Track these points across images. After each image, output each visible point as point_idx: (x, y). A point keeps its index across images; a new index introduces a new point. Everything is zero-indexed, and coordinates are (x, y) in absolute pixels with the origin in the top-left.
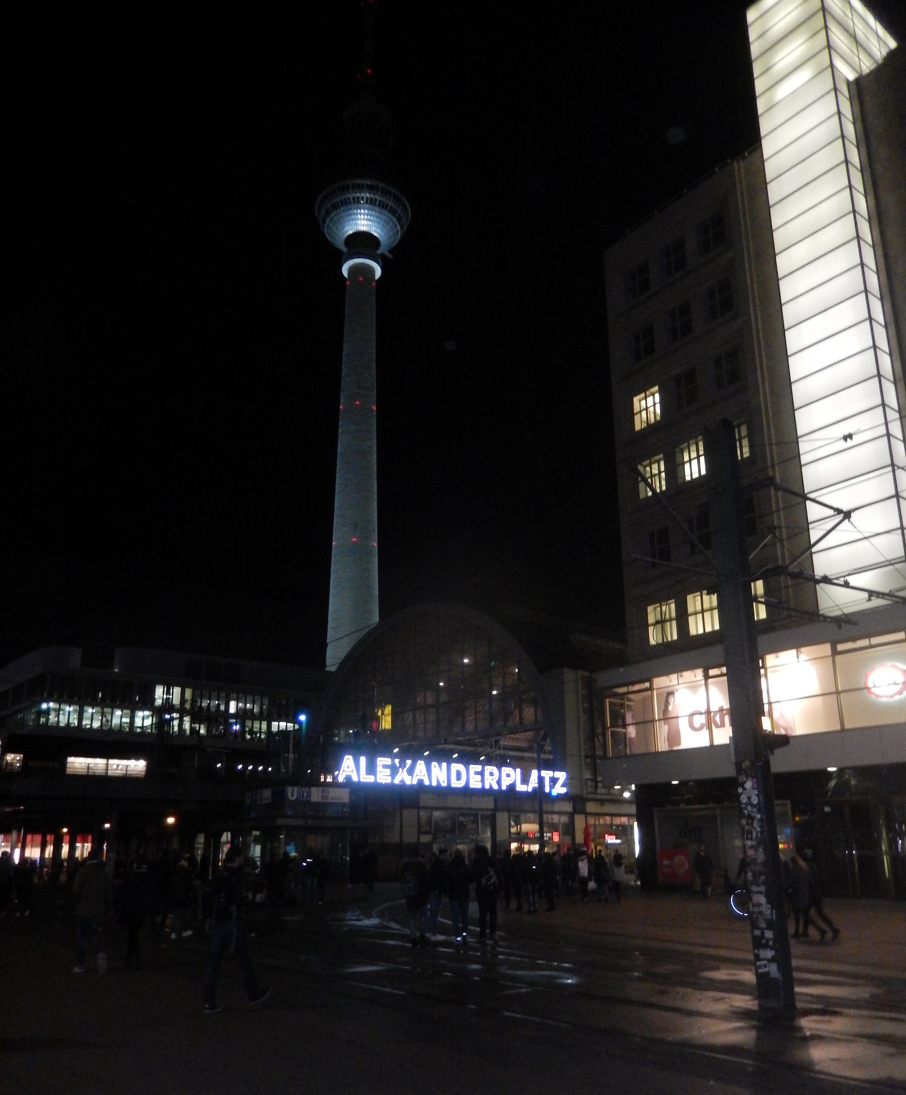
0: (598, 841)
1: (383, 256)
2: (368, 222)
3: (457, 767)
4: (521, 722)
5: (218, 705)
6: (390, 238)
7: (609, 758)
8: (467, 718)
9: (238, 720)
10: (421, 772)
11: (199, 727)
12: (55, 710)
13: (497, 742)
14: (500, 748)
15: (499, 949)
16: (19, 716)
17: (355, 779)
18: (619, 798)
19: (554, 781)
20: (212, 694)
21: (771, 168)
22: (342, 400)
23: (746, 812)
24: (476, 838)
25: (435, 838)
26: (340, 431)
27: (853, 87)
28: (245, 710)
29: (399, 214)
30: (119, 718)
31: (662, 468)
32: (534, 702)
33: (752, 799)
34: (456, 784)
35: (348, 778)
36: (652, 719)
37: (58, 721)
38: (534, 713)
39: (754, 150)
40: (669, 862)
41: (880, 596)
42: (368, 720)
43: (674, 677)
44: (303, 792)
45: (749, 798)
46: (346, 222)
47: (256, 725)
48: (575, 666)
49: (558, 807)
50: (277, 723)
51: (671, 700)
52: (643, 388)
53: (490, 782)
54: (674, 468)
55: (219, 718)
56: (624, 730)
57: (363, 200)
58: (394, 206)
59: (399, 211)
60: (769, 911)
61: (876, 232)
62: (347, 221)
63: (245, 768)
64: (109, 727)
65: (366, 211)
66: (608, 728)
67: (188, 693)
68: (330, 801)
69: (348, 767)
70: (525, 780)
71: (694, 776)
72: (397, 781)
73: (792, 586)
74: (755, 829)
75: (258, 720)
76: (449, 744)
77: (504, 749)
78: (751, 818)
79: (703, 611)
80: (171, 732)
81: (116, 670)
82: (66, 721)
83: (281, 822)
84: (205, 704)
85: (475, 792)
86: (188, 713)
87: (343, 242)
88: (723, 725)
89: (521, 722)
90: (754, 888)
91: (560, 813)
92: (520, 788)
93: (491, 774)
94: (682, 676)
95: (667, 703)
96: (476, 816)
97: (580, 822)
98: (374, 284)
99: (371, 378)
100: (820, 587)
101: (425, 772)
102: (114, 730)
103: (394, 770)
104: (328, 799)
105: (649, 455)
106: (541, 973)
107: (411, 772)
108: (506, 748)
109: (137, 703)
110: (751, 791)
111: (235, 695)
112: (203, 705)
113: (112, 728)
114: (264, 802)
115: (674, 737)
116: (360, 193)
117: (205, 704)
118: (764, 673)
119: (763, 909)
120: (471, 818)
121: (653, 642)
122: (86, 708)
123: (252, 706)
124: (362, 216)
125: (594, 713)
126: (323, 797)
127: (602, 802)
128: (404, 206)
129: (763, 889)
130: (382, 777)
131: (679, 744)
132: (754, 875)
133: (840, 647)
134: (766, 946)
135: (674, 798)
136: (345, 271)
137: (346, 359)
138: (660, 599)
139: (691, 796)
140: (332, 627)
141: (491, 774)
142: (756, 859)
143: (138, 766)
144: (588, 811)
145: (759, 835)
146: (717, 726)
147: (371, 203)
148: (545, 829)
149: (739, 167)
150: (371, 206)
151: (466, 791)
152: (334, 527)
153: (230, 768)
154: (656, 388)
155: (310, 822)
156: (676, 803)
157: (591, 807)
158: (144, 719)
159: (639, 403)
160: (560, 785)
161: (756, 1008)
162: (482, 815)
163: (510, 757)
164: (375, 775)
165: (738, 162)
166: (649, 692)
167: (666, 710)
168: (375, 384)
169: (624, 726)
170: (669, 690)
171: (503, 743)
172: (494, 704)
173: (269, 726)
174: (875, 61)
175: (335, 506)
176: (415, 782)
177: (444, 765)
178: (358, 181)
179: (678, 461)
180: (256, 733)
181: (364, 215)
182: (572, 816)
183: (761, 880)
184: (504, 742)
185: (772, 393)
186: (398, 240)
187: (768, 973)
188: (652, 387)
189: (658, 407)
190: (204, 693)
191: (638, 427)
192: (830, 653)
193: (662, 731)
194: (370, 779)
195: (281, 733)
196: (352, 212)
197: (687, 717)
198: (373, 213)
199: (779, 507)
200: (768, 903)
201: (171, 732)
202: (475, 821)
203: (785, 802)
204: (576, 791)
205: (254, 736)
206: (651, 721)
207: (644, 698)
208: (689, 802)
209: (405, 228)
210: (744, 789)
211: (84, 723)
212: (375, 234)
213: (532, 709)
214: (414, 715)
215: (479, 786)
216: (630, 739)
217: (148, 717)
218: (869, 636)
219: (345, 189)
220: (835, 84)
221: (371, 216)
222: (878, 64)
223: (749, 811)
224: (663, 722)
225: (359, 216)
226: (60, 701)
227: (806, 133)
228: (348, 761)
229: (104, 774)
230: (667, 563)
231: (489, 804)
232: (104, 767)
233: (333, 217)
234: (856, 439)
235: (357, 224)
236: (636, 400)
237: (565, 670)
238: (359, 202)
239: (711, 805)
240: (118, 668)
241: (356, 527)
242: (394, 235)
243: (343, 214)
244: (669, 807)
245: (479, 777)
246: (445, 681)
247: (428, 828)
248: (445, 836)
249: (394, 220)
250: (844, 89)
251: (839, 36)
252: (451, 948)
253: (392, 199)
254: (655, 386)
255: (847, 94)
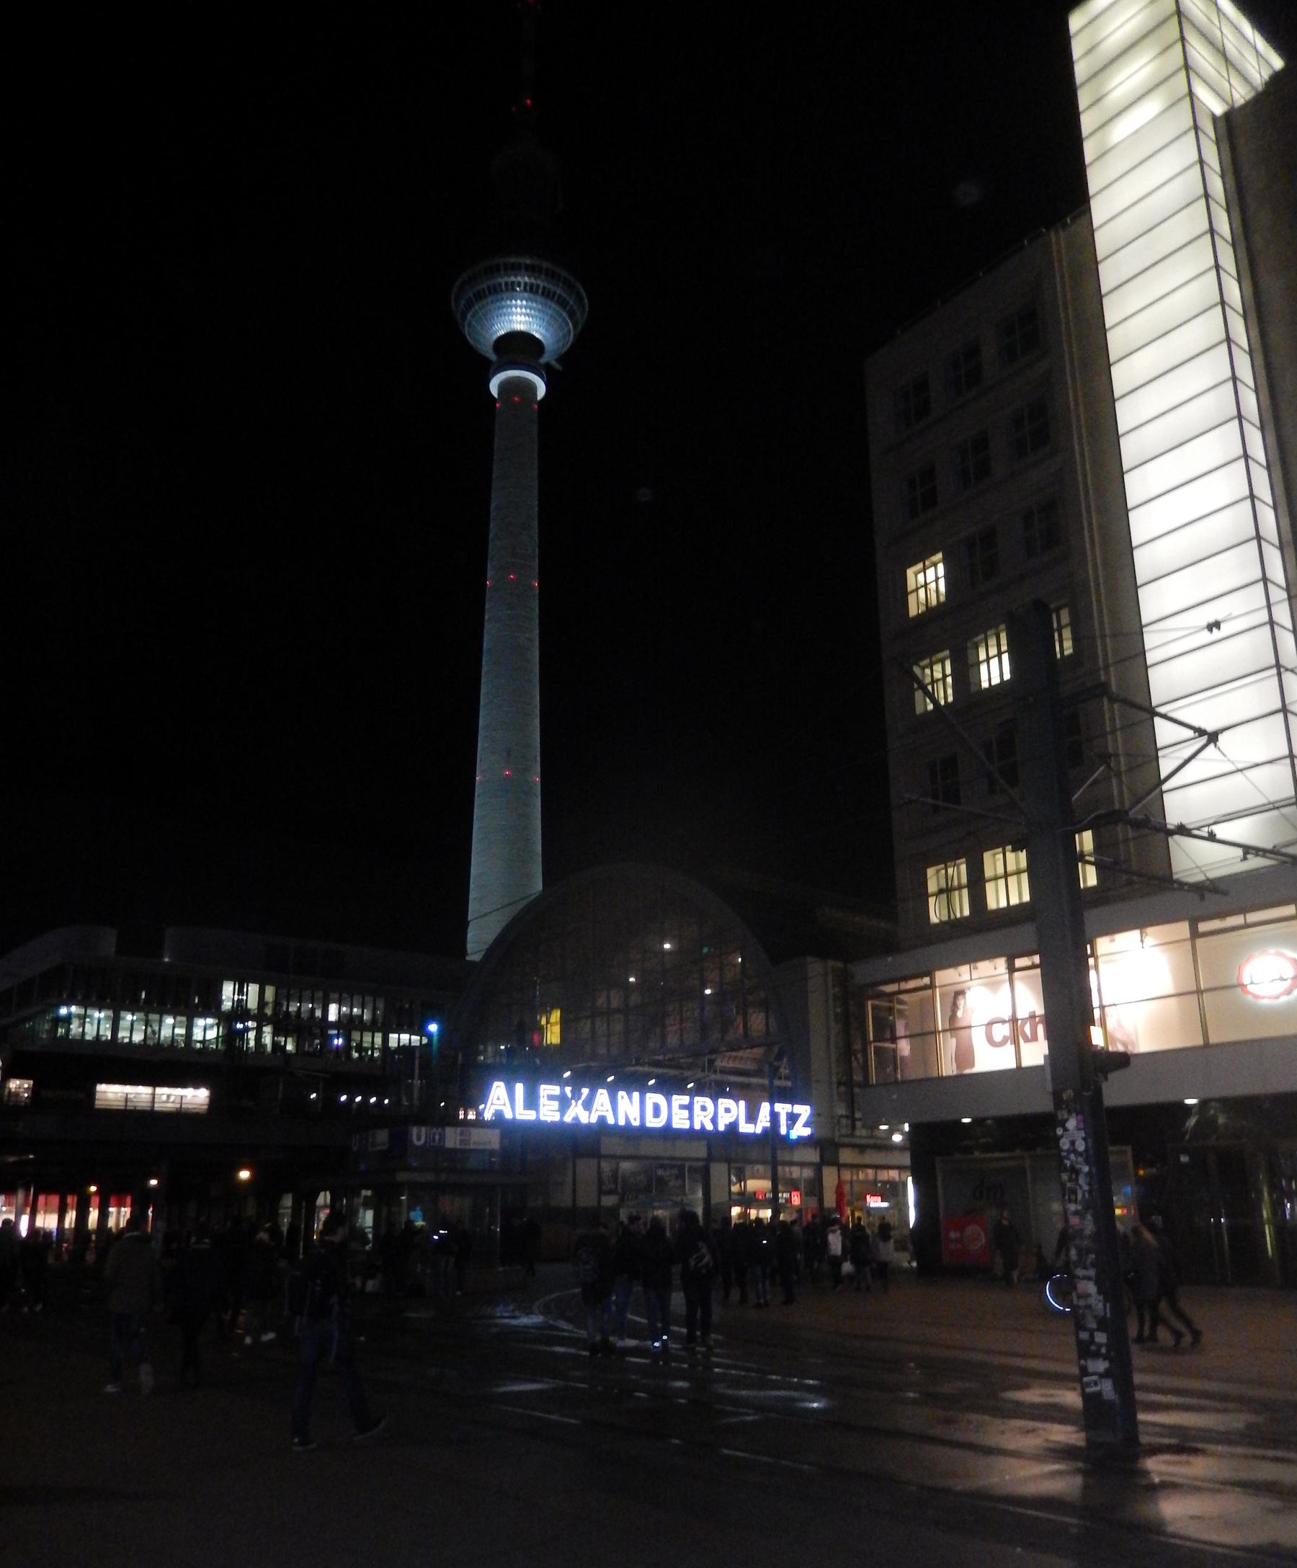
0: (855, 1204)
1: (548, 367)
2: (527, 318)
3: (654, 1098)
4: (746, 1034)
5: (313, 1010)
6: (558, 341)
7: (872, 1085)
8: (669, 1029)
9: (341, 1031)
10: (602, 1105)
11: (286, 1041)
12: (79, 1016)
13: (711, 1062)
14: (715, 1072)
15: (714, 1359)
16: (27, 1026)
17: (508, 1115)
18: (886, 1142)
19: (793, 1118)
20: (304, 993)
21: (1103, 241)
22: (490, 573)
23: (1068, 1163)
24: (682, 1200)
25: (622, 1200)
26: (486, 617)
27: (1222, 125)
28: (350, 1017)
29: (572, 306)
30: (170, 1027)
31: (948, 671)
32: (765, 1006)
33: (1077, 1144)
34: (653, 1123)
35: (499, 1114)
36: (933, 1029)
37: (83, 1033)
38: (764, 1021)
39: (1079, 215)
40: (958, 1235)
41: (1260, 853)
42: (527, 1031)
43: (964, 969)
44: (434, 1134)
45: (1073, 1143)
46: (495, 318)
47: (367, 1038)
48: (823, 954)
49: (799, 1155)
50: (396, 1036)
51: (961, 1002)
52: (920, 556)
53: (702, 1120)
54: (965, 671)
55: (314, 1028)
56: (893, 1046)
57: (519, 286)
58: (564, 295)
59: (571, 302)
60: (1101, 1305)
61: (1255, 333)
62: (497, 317)
63: (351, 1100)
64: (156, 1041)
65: (524, 302)
66: (871, 1043)
67: (270, 992)
68: (472, 1147)
69: (498, 1099)
70: (752, 1117)
71: (994, 1112)
72: (568, 1118)
73: (1134, 839)
74: (1081, 1187)
75: (369, 1031)
76: (642, 1065)
77: (721, 1072)
78: (1074, 1171)
79: (1006, 875)
80: (245, 1049)
81: (166, 960)
82: (95, 1033)
83: (402, 1177)
84: (293, 1008)
85: (680, 1134)
86: (269, 1021)
87: (492, 346)
88: (1034, 1038)
89: (746, 1034)
90: (1080, 1272)
91: (802, 1165)
92: (745, 1128)
93: (704, 1108)
94: (976, 968)
95: (955, 1007)
96: (681, 1168)
97: (830, 1177)
98: (536, 407)
99: (531, 541)
100: (1174, 841)
101: (608, 1105)
102: (163, 1045)
103: (564, 1103)
104: (469, 1145)
105: (929, 652)
106: (774, 1393)
107: (588, 1105)
108: (724, 1071)
109: (197, 1006)
110: (1076, 1132)
111: (336, 996)
112: (291, 1009)
113: (161, 1042)
114: (378, 1148)
115: (965, 1055)
116: (516, 277)
117: (293, 1008)
118: (1093, 963)
119: (1092, 1301)
120: (675, 1172)
121: (934, 919)
122: (123, 1014)
123: (360, 1010)
124: (519, 310)
125: (850, 1021)
126: (462, 1141)
127: (862, 1148)
128: (578, 295)
129: (1092, 1272)
130: (547, 1113)
131: (973, 1065)
132: (1080, 1254)
133: (1203, 927)
134: (1096, 1355)
135: (965, 1143)
136: (494, 388)
137: (495, 514)
138: (945, 858)
139: (990, 1140)
140: (475, 899)
141: (704, 1108)
142: (1082, 1230)
143: (197, 1097)
144: (841, 1161)
145: (1087, 1196)
146: (1027, 1040)
147: (531, 291)
148: (780, 1187)
149: (1058, 239)
150: (531, 295)
151: (668, 1133)
152: (478, 754)
153: (329, 1100)
154: (939, 556)
155: (443, 1177)
156: (968, 1150)
157: (846, 1156)
158: (206, 1030)
159: (914, 576)
160: (802, 1124)
161: (1082, 1443)
162: (690, 1167)
163: (730, 1084)
164: (537, 1110)
165: (1057, 232)
166: (930, 991)
167: (953, 1017)
168: (537, 549)
169: (894, 1039)
170: (958, 988)
171: (721, 1064)
172: (707, 1008)
173: (385, 1040)
174: (1253, 88)
175: (480, 725)
176: (594, 1120)
177: (636, 1095)
178: (513, 260)
179: (971, 660)
180: (366, 1050)
181: (521, 308)
182: (818, 1168)
183: (1089, 1260)
184: (722, 1062)
185: (1105, 563)
186: (570, 343)
187: (1099, 1394)
188: (934, 554)
189: (942, 583)
190: (292, 992)
191: (913, 611)
192: (1188, 935)
193: (948, 1046)
194: (530, 1116)
195: (402, 1049)
196: (503, 303)
197: (984, 1027)
198: (534, 305)
199: (1115, 726)
200: (1099, 1292)
201: (245, 1049)
202: (680, 1176)
203: (1124, 1148)
204: (825, 1133)
205: (363, 1054)
206: (932, 1033)
207: (922, 1000)
208: (987, 1148)
209: (580, 327)
210: (1066, 1130)
211: (120, 1035)
212: (537, 335)
213: (762, 1015)
214: (593, 1023)
215: (686, 1125)
216: (902, 1058)
217: (212, 1027)
218: (1244, 911)
219: (494, 270)
220: (1195, 120)
221: (530, 310)
222: (1256, 91)
223: (1072, 1162)
224: (949, 1033)
225: (514, 309)
226: (85, 1003)
227: (1153, 191)
228: (498, 1090)
229: (149, 1109)
230: (955, 807)
231: (700, 1151)
232: (149, 1098)
233: (476, 311)
234: (1226, 629)
235: (511, 321)
236: (910, 572)
237: (809, 959)
238: (514, 290)
239: (1018, 1152)
240: (169, 957)
241: (509, 755)
242: (564, 336)
243: (492, 307)
244: (957, 1156)
245: (686, 1113)
246: (637, 975)
247: (613, 1186)
248: (637, 1197)
249: (564, 314)
250: (1208, 127)
251: (1202, 52)
252: (646, 1358)
253: (561, 285)
254: (938, 552)
255: (1212, 135)
